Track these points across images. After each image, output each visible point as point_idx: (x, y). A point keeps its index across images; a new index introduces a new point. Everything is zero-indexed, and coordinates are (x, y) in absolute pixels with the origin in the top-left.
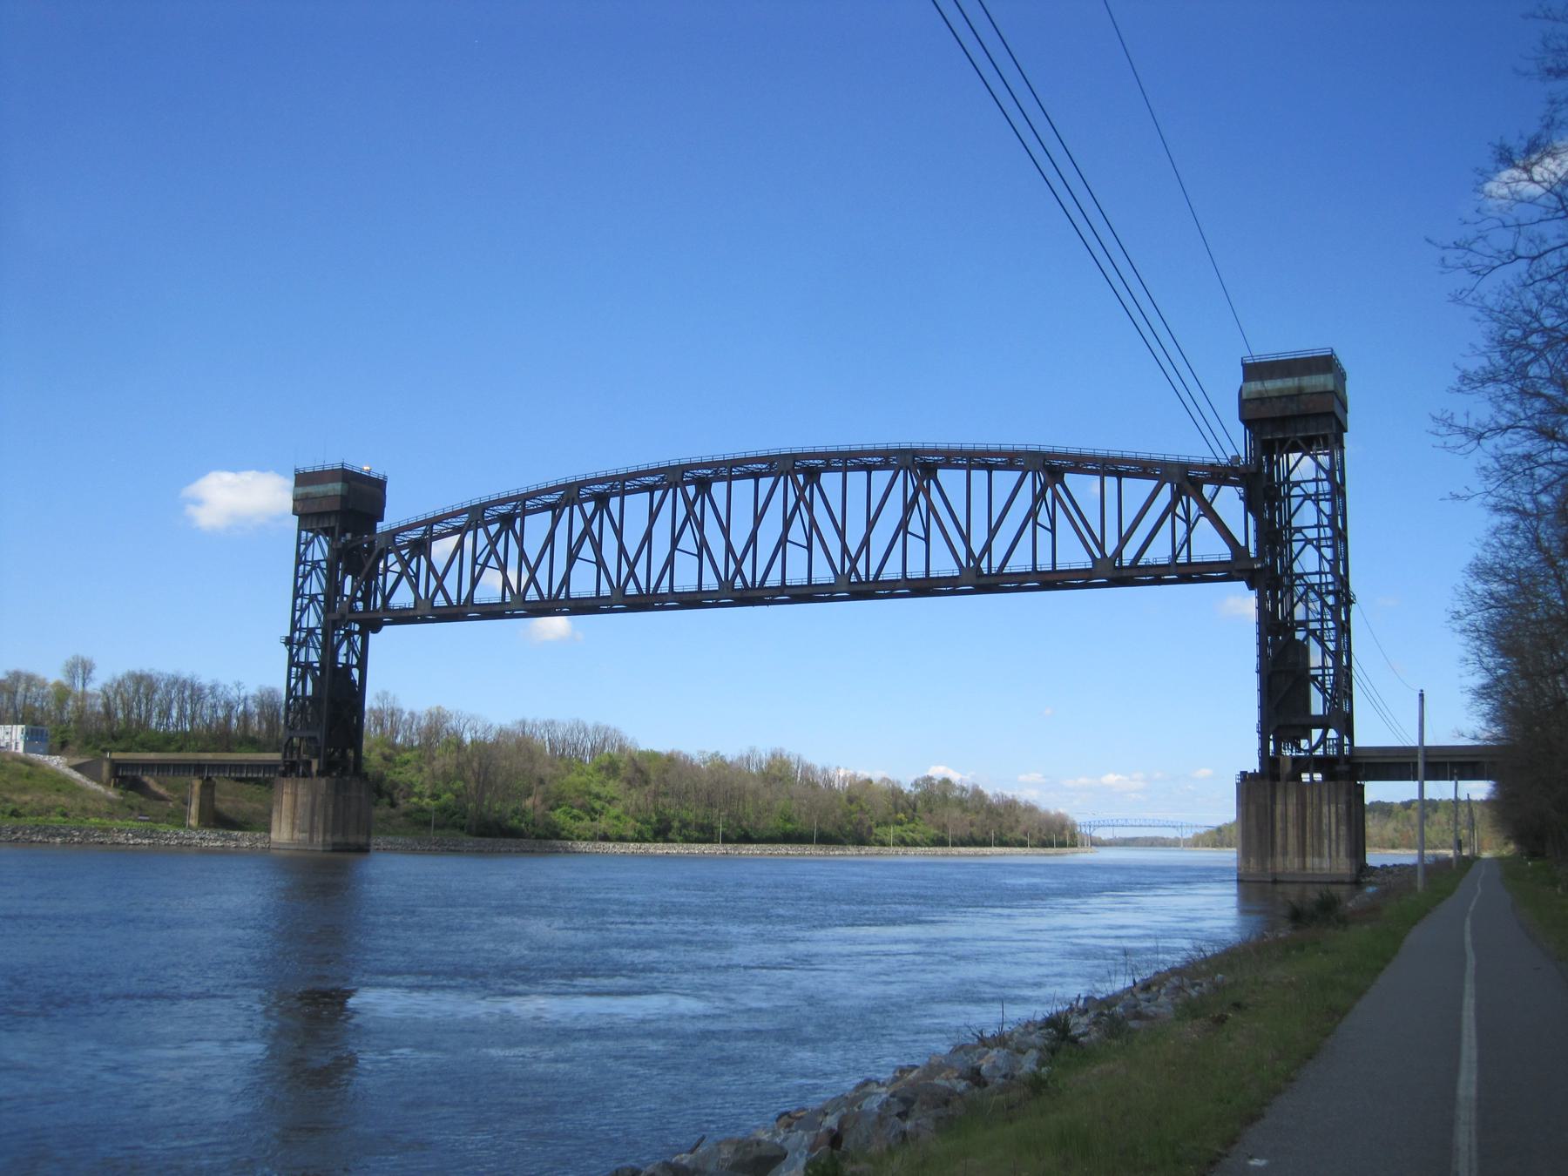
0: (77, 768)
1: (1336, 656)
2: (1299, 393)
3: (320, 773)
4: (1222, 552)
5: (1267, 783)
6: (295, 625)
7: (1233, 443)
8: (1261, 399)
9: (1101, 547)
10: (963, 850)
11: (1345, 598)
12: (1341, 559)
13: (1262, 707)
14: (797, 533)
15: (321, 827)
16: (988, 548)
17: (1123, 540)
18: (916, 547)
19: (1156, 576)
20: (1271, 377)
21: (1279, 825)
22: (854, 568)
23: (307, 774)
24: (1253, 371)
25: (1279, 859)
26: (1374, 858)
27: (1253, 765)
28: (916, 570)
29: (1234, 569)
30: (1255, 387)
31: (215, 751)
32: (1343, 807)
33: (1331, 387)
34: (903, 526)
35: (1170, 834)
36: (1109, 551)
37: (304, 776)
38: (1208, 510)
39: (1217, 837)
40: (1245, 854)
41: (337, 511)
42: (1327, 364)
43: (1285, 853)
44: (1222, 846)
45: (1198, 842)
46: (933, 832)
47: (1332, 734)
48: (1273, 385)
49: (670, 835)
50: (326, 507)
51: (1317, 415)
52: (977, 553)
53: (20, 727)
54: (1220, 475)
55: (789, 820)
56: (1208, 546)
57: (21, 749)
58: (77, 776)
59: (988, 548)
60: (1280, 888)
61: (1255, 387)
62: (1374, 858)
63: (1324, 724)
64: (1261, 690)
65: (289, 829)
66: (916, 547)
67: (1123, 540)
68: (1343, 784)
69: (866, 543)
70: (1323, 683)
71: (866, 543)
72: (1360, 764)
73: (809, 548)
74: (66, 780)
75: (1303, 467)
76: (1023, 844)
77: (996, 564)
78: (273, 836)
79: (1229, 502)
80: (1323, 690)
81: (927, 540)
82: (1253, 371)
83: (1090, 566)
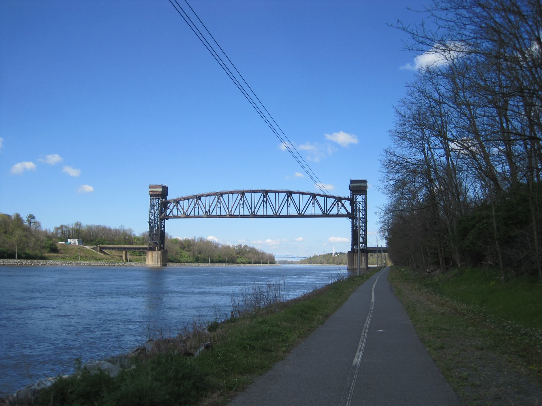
0: (92, 249)
1: (364, 232)
2: (360, 186)
3: (158, 250)
4: (346, 213)
5: (353, 253)
6: (150, 219)
7: (347, 194)
8: (353, 187)
9: (299, 211)
10: (256, 264)
11: (366, 222)
12: (365, 216)
13: (352, 240)
14: (197, 206)
15: (160, 261)
16: (254, 211)
17: (302, 211)
18: (197, 210)
19: (237, 217)
20: (355, 183)
21: (354, 260)
22: (207, 214)
23: (155, 250)
24: (352, 182)
25: (354, 266)
26: (369, 266)
27: (350, 250)
28: (197, 214)
29: (348, 216)
30: (352, 185)
31: (123, 245)
32: (365, 257)
33: (365, 186)
34: (194, 207)
35: (294, 260)
36: (301, 212)
37: (154, 250)
38: (343, 205)
39: (310, 261)
40: (349, 265)
41: (160, 195)
42: (365, 182)
43: (355, 265)
44: (311, 263)
45: (302, 262)
46: (248, 260)
47: (363, 245)
48: (355, 185)
49: (199, 262)
50: (158, 193)
51: (363, 190)
52: (230, 211)
53: (77, 239)
54: (346, 199)
55: (220, 257)
56: (343, 212)
57: (77, 244)
58: (92, 250)
59: (254, 211)
60: (354, 271)
61: (352, 185)
62: (369, 266)
63: (362, 243)
64: (352, 237)
65: (151, 261)
66: (197, 210)
67: (302, 211)
68: (365, 253)
69: (209, 210)
70: (362, 236)
71: (209, 210)
72: (368, 250)
73: (199, 208)
74: (90, 250)
75: (360, 199)
76: (266, 263)
77: (279, 213)
78: (147, 263)
79: (347, 204)
80: (362, 238)
81: (221, 208)
82: (352, 182)
83: (347, 214)
